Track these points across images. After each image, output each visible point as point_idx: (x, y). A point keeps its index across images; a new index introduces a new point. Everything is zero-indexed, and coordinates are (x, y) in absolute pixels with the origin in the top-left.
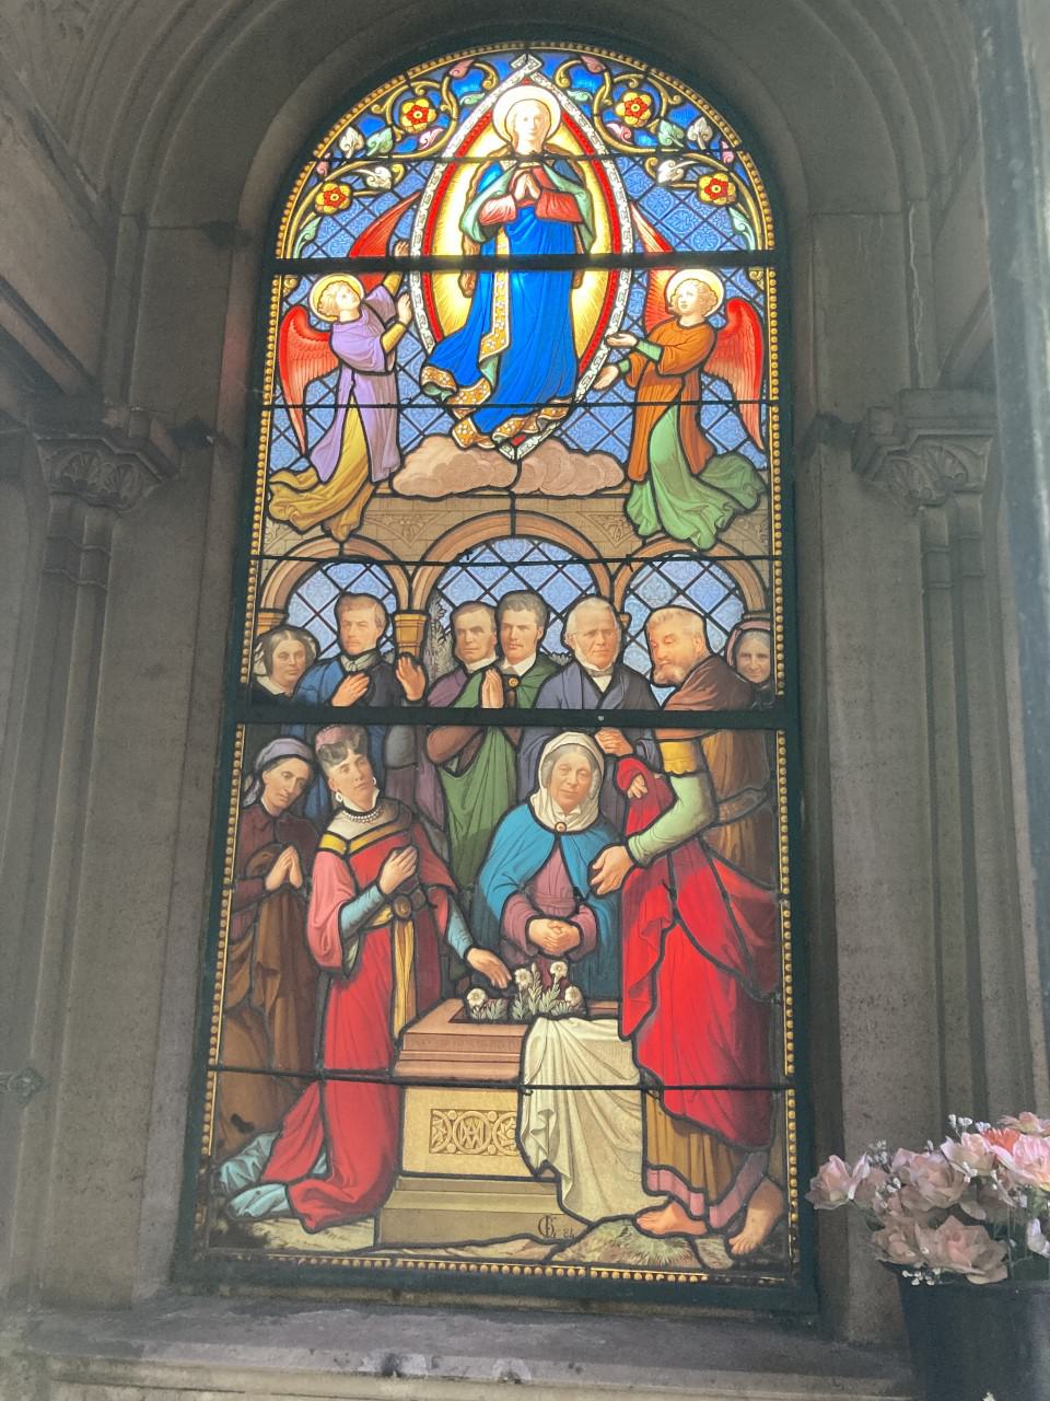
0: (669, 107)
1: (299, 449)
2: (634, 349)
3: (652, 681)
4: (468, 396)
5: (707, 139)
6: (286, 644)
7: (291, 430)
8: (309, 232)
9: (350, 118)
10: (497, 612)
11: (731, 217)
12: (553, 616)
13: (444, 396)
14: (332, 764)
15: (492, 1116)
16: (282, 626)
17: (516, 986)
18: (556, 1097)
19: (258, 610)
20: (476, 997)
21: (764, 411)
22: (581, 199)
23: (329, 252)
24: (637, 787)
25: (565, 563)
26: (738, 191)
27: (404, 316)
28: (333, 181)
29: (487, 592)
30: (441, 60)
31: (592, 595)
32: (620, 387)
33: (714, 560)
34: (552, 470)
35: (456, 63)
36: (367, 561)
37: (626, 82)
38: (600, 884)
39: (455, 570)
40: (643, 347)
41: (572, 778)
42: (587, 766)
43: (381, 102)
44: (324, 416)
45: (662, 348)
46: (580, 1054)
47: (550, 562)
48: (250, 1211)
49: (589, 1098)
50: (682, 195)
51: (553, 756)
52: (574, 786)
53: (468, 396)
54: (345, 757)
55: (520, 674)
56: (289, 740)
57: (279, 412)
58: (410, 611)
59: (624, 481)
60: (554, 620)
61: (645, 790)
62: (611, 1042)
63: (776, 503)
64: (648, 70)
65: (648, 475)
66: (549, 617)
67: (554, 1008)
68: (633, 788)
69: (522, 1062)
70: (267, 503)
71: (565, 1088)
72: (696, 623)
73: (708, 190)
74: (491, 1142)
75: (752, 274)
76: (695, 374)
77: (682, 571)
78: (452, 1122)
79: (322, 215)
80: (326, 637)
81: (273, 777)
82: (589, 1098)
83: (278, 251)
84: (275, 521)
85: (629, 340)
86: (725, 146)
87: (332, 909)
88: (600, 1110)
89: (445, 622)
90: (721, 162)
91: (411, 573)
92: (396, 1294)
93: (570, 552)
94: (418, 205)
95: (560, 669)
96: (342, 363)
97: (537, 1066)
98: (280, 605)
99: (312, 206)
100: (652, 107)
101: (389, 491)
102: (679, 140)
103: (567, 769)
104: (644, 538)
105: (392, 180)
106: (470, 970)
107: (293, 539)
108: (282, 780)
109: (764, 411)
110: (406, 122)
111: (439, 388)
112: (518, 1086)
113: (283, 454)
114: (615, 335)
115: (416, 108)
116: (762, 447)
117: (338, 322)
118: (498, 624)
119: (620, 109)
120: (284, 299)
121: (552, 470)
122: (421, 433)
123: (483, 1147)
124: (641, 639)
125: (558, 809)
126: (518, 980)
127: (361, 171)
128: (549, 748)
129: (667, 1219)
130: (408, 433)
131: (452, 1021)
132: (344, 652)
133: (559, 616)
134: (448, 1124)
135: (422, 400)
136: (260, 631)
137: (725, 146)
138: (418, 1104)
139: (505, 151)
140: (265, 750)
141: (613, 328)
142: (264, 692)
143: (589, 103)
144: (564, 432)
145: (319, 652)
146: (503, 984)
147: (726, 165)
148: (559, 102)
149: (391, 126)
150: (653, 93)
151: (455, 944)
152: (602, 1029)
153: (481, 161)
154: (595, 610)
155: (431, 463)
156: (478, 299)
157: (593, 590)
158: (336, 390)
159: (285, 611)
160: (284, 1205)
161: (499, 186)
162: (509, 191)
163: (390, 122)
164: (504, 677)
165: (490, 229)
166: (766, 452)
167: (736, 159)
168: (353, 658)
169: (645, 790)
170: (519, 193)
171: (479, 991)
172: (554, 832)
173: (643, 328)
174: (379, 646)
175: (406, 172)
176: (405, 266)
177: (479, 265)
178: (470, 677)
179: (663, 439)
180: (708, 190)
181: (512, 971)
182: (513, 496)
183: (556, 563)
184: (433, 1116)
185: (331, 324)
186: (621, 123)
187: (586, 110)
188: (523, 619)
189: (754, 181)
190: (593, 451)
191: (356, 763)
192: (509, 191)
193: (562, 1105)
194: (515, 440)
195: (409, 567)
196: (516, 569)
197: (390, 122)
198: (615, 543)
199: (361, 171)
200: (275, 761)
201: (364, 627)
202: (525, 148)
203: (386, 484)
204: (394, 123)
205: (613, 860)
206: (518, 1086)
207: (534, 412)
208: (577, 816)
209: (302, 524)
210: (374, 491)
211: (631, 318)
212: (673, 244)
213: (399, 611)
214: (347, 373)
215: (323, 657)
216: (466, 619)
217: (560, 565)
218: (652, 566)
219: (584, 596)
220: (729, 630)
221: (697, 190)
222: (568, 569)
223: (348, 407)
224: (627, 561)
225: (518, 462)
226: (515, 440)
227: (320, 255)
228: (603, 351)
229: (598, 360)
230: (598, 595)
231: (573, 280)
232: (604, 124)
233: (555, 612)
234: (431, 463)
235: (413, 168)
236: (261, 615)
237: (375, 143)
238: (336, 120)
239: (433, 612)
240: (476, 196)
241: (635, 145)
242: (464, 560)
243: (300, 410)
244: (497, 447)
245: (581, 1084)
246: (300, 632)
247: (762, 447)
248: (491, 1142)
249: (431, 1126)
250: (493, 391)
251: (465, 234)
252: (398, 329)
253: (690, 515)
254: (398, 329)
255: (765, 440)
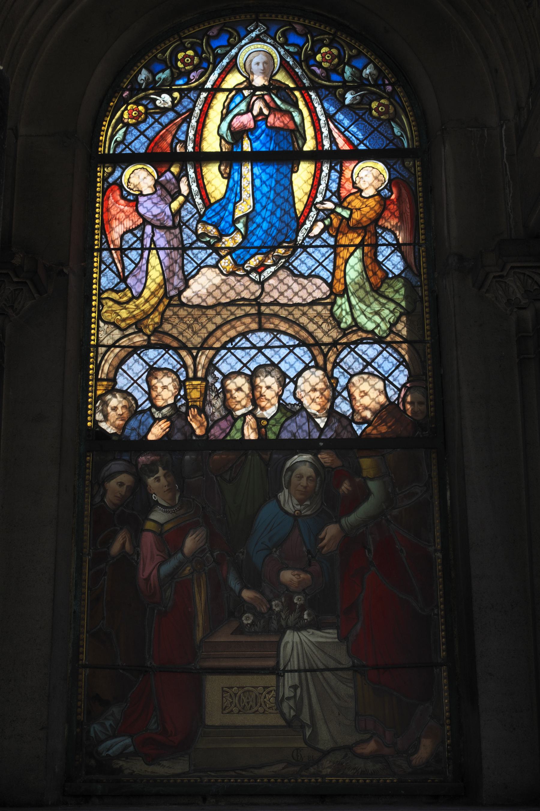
0: (350, 57)
1: (118, 275)
2: (333, 211)
3: (353, 420)
4: (228, 242)
5: (375, 77)
6: (115, 401)
7: (113, 265)
8: (119, 136)
9: (144, 62)
10: (251, 379)
11: (392, 128)
12: (288, 380)
13: (212, 241)
14: (149, 477)
15: (261, 689)
16: (113, 390)
17: (273, 610)
18: (300, 677)
19: (97, 380)
20: (247, 619)
21: (417, 250)
22: (295, 114)
23: (133, 149)
24: (345, 486)
25: (295, 346)
26: (395, 110)
27: (184, 190)
28: (133, 103)
29: (245, 365)
30: (201, 25)
31: (312, 367)
32: (325, 236)
33: (389, 344)
34: (284, 289)
35: (212, 27)
36: (166, 347)
37: (322, 40)
38: (323, 547)
39: (223, 352)
40: (339, 210)
41: (304, 482)
42: (313, 474)
43: (164, 52)
44: (134, 255)
45: (351, 210)
46: (314, 651)
47: (284, 346)
48: (110, 752)
49: (321, 677)
50: (361, 113)
51: (292, 468)
52: (305, 487)
53: (228, 242)
54: (157, 472)
55: (268, 418)
56: (120, 462)
57: (105, 254)
58: (195, 378)
59: (330, 295)
60: (289, 383)
61: (350, 489)
62: (334, 642)
63: (426, 307)
64: (335, 33)
65: (346, 290)
66: (285, 381)
67: (297, 623)
68: (343, 488)
69: (278, 656)
70: (99, 311)
71: (306, 671)
72: (380, 385)
73: (376, 110)
74: (261, 706)
75: (406, 163)
76: (372, 228)
77: (370, 351)
78: (235, 695)
79: (127, 125)
80: (140, 395)
81: (113, 484)
82: (321, 677)
83: (100, 149)
84: (105, 323)
85: (329, 205)
86: (387, 82)
87: (151, 566)
88: (328, 683)
89: (218, 385)
90: (384, 91)
91: (195, 354)
92: (204, 799)
93: (298, 339)
94: (191, 120)
95: (295, 414)
96: (146, 222)
97: (288, 658)
98: (111, 375)
99: (121, 119)
100: (339, 56)
101: (179, 302)
102: (357, 78)
103: (301, 477)
104: (344, 330)
105: (173, 102)
106: (242, 601)
107: (117, 334)
108: (117, 485)
109: (417, 250)
110: (180, 65)
111: (209, 237)
112: (277, 671)
113: (108, 280)
114: (322, 203)
115: (186, 56)
116: (416, 272)
117: (141, 194)
118: (253, 387)
119: (319, 57)
120: (105, 179)
121: (284, 289)
122: (199, 265)
123: (256, 709)
124: (345, 394)
125: (295, 502)
126: (274, 608)
127: (152, 96)
128: (289, 464)
129: (371, 747)
130: (189, 268)
131: (232, 634)
132: (154, 405)
133: (292, 380)
134: (233, 695)
135: (200, 244)
136: (99, 393)
137: (387, 82)
138: (214, 686)
139: (245, 83)
140: (105, 469)
141: (319, 198)
142: (103, 431)
143: (299, 53)
144: (291, 264)
145: (138, 406)
146: (264, 609)
147: (388, 93)
148: (279, 53)
149: (170, 68)
150: (339, 47)
151: (233, 586)
152: (328, 635)
153: (230, 90)
154: (315, 377)
155: (204, 284)
156: (231, 181)
157: (313, 364)
158: (141, 239)
159: (114, 381)
160: (131, 749)
161: (243, 106)
162: (249, 109)
163: (169, 65)
164: (258, 420)
165: (238, 135)
166: (419, 275)
167: (394, 90)
168: (159, 409)
169: (350, 489)
170: (256, 112)
171: (250, 615)
172: (293, 516)
173: (339, 197)
174: (176, 401)
175: (181, 98)
176: (184, 159)
177: (230, 159)
178: (236, 419)
179: (354, 268)
180: (376, 110)
181: (270, 601)
182: (259, 305)
183: (288, 347)
184: (223, 691)
185: (137, 196)
186: (319, 65)
187: (297, 57)
188: (268, 383)
189: (406, 104)
190: (310, 276)
191: (165, 476)
192: (249, 109)
193: (304, 682)
194: (260, 268)
195: (194, 351)
196: (263, 350)
197: (169, 65)
198: (325, 334)
199: (152, 96)
200: (112, 476)
201: (166, 390)
202: (259, 81)
203: (176, 298)
204: (172, 65)
205: (331, 531)
206: (277, 671)
207: (270, 251)
208: (308, 506)
209: (123, 325)
210: (169, 303)
211: (331, 191)
212: (356, 143)
213: (188, 379)
214: (148, 229)
215: (140, 409)
216: (231, 385)
217: (291, 349)
218: (350, 348)
219: (307, 367)
220: (399, 387)
221: (371, 109)
222: (297, 351)
223: (150, 249)
224: (335, 343)
225: (261, 284)
226: (260, 268)
227: (127, 151)
228: (313, 214)
229: (311, 218)
230: (317, 367)
231: (293, 168)
232: (309, 67)
233: (289, 377)
234: (204, 284)
235: (186, 95)
236: (99, 383)
237: (160, 78)
238: (135, 65)
239: (210, 379)
240: (229, 112)
241: (329, 80)
242: (230, 345)
243: (119, 252)
244: (248, 274)
245: (316, 668)
246: (126, 394)
247: (416, 272)
248: (261, 706)
249: (223, 697)
250: (244, 237)
251: (221, 137)
252: (181, 199)
253: (374, 316)
254: (181, 199)
255: (418, 267)
